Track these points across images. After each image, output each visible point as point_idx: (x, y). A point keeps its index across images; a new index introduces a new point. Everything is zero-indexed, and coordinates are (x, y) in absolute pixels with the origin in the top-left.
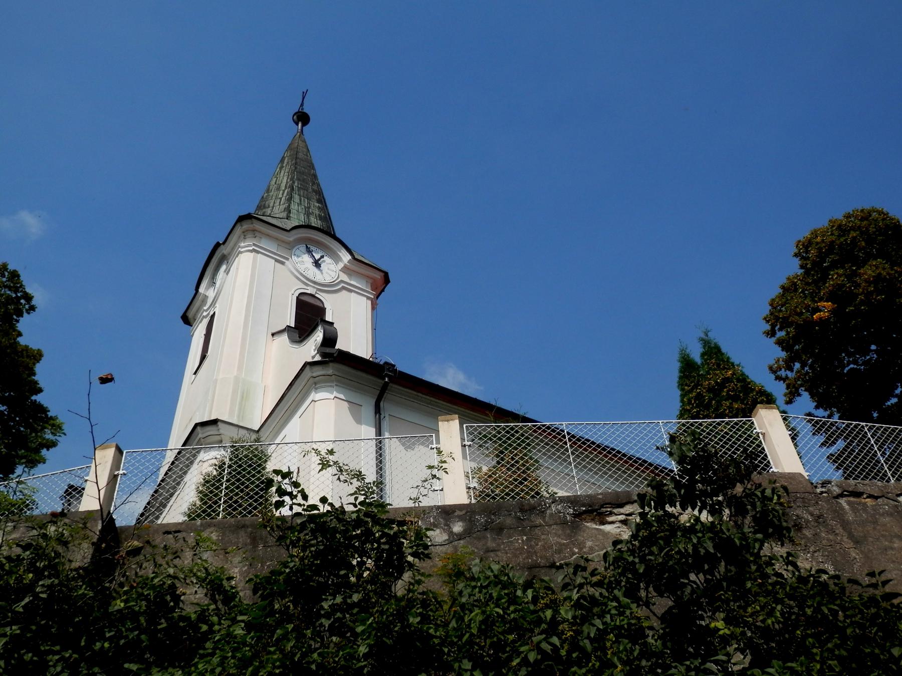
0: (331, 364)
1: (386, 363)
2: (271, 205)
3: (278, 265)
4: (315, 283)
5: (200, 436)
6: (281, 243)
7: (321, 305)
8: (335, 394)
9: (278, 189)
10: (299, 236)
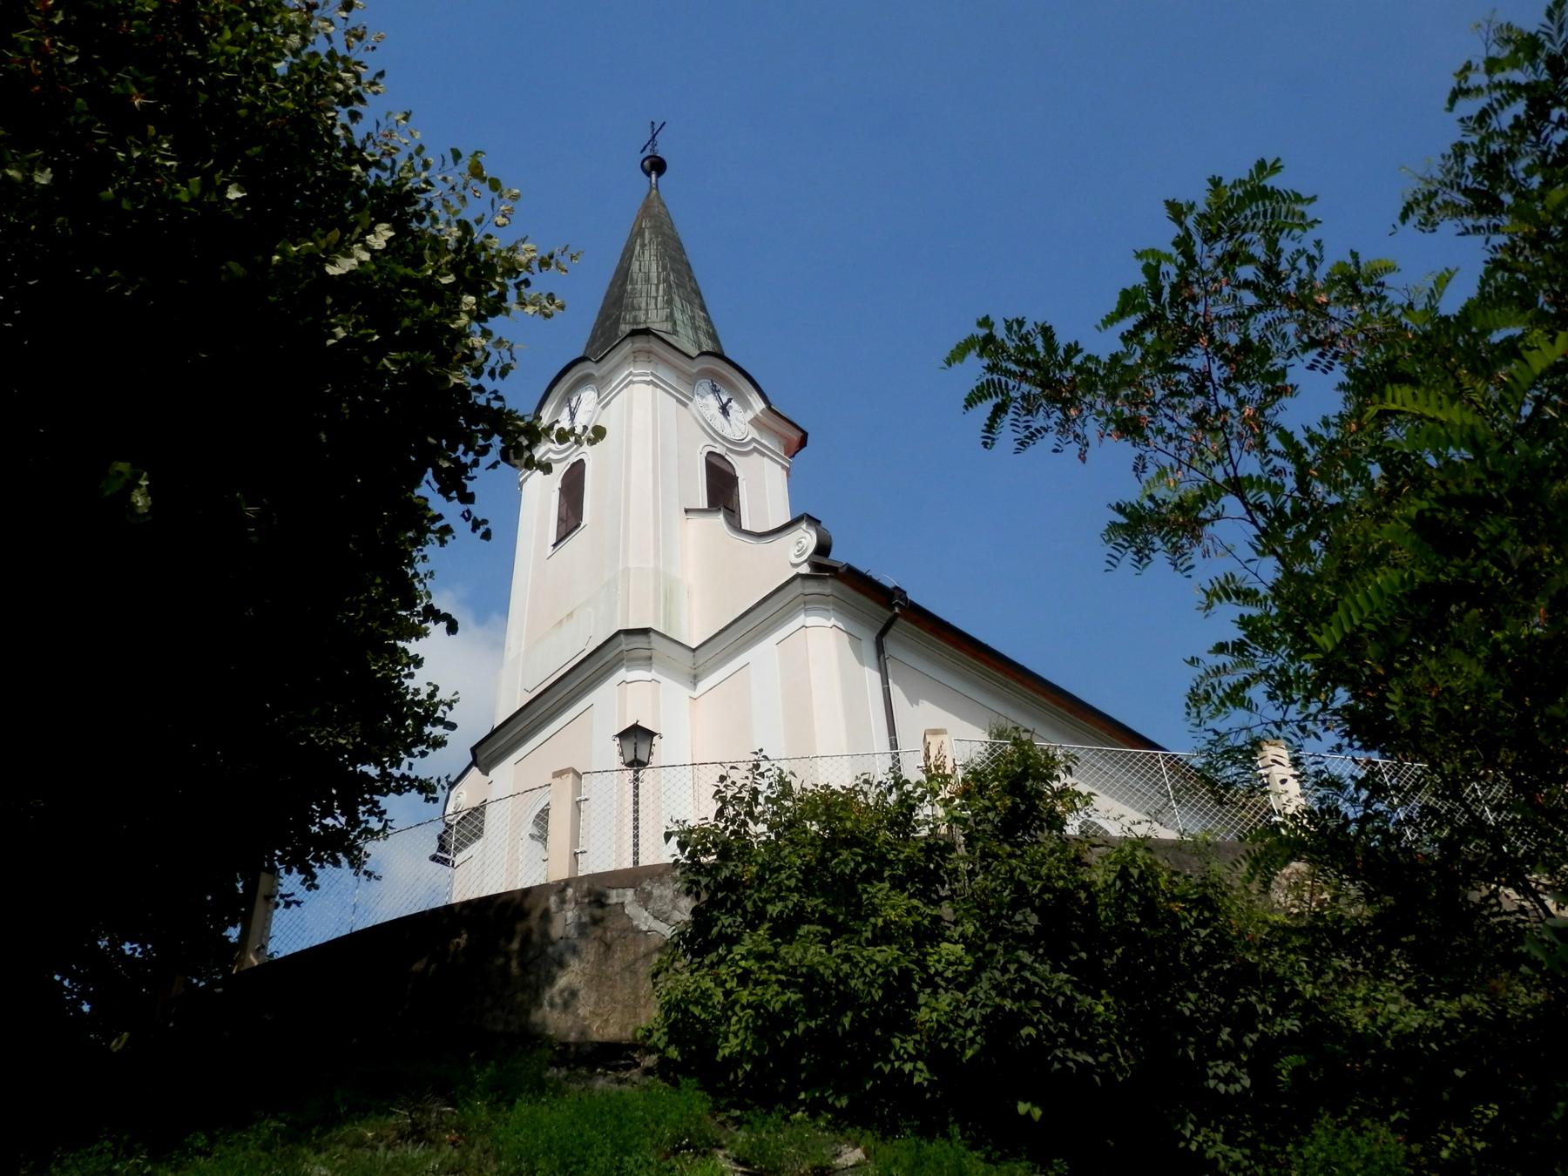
0: (830, 581)
2: (643, 305)
4: (724, 438)
8: (833, 621)
9: (648, 280)
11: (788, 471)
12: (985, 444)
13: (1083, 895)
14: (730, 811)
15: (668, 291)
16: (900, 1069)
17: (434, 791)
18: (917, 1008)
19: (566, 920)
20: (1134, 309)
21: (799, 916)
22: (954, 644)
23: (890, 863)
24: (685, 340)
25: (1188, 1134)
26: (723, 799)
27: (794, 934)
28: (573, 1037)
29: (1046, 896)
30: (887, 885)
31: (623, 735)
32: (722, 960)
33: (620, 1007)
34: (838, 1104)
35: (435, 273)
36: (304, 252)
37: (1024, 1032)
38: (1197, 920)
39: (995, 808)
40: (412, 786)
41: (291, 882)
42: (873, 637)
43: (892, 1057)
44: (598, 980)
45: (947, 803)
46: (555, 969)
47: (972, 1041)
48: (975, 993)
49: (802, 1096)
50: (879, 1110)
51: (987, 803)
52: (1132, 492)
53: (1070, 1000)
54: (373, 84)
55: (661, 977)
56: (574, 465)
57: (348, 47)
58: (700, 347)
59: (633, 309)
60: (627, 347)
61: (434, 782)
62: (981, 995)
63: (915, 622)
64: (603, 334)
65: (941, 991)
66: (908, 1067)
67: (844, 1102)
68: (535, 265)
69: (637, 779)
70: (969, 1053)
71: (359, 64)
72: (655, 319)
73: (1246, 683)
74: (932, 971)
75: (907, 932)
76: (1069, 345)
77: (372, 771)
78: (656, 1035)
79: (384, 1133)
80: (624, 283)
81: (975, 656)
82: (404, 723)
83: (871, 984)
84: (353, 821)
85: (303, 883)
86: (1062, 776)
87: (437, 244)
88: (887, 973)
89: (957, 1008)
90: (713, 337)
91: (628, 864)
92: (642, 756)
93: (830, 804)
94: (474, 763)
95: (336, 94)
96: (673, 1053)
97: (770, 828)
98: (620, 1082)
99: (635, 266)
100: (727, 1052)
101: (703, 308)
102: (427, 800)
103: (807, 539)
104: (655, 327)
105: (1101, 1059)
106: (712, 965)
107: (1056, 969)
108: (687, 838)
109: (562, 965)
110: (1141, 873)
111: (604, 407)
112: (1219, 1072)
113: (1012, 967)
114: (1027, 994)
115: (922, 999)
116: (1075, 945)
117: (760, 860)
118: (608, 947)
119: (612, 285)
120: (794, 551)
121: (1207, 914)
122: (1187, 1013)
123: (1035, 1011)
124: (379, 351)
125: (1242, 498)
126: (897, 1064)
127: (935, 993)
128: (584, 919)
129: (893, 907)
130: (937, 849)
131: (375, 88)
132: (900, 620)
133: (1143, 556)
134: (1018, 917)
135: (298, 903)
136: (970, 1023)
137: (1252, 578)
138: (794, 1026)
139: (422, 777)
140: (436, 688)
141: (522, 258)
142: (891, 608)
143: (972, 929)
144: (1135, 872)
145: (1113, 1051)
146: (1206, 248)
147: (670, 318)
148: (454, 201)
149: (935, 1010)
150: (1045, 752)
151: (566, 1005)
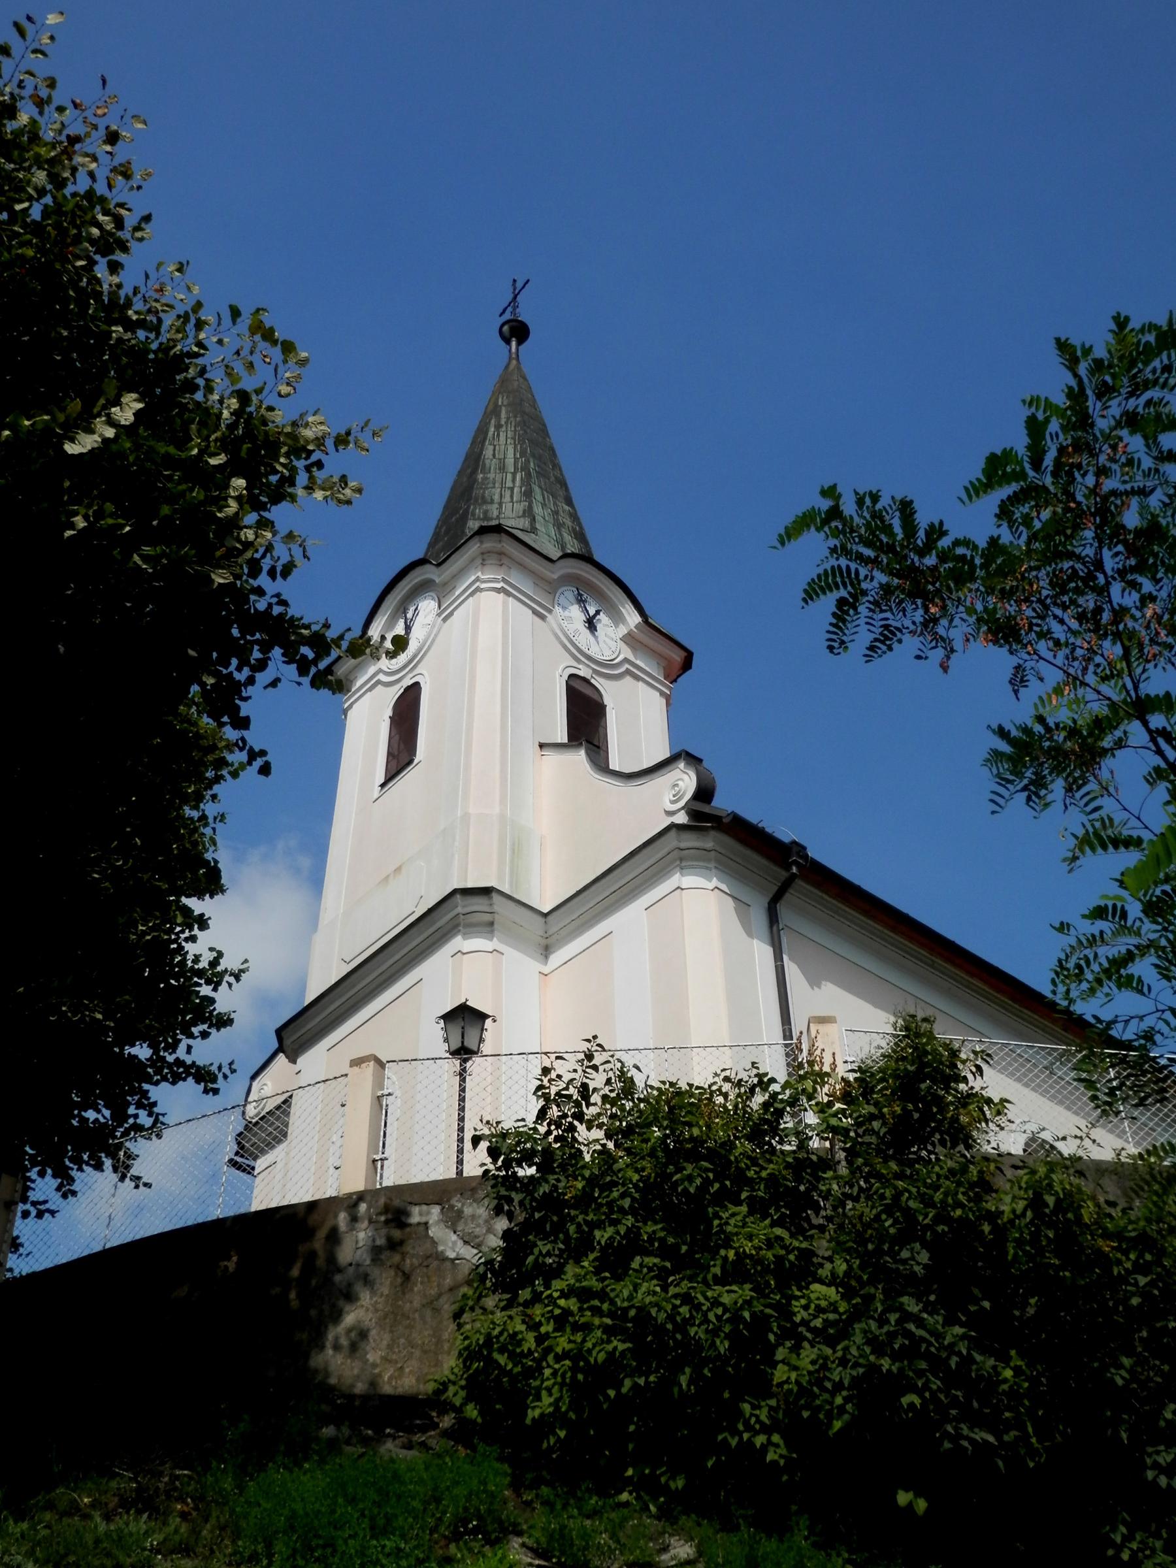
0: (713, 833)
1: (794, 842)
3: (537, 619)
4: (589, 658)
6: (539, 580)
7: (598, 699)
8: (715, 882)
9: (502, 468)
10: (570, 571)
11: (668, 699)
12: (831, 648)
13: (986, 1228)
14: (554, 1112)
15: (527, 481)
16: (750, 1442)
17: (214, 1079)
18: (774, 1365)
19: (357, 1242)
20: (1007, 479)
21: (633, 1245)
22: (865, 913)
23: (750, 1182)
24: (545, 539)
25: (1118, 1539)
26: (546, 1097)
27: (627, 1268)
28: (360, 1388)
29: (940, 1228)
30: (744, 1209)
31: (448, 1017)
32: (536, 1298)
33: (417, 1353)
34: (672, 1485)
35: (202, 452)
36: (39, 427)
37: (905, 1400)
38: (1135, 1263)
39: (882, 1116)
40: (189, 1074)
41: (44, 1187)
42: (764, 901)
43: (741, 1427)
44: (393, 1317)
45: (822, 1109)
46: (341, 1303)
47: (842, 1410)
48: (846, 1349)
49: (630, 1472)
50: (721, 1494)
51: (872, 1109)
52: (1018, 713)
53: (967, 1361)
54: (137, 228)
55: (466, 1317)
56: (408, 689)
57: (110, 187)
58: (563, 548)
59: (485, 502)
60: (474, 548)
61: (214, 1068)
62: (854, 1351)
63: (818, 885)
64: (447, 532)
65: (806, 1344)
66: (760, 1440)
67: (680, 1483)
68: (329, 443)
69: (464, 1070)
70: (837, 1425)
71: (122, 205)
72: (511, 515)
73: (1129, 957)
74: (798, 1319)
75: (766, 1270)
76: (932, 526)
77: (142, 1052)
78: (452, 1389)
79: (104, 1499)
80: (474, 472)
81: (893, 929)
82: (177, 1001)
83: (715, 1333)
84: (120, 1115)
85: (58, 1189)
86: (970, 1077)
87: (208, 418)
88: (736, 1319)
89: (824, 1367)
90: (581, 536)
91: (452, 1174)
92: (471, 1043)
93: (677, 1104)
94: (280, 1049)
95: (92, 241)
96: (472, 1412)
97: (608, 1136)
98: (409, 1446)
99: (488, 452)
100: (537, 1413)
101: (569, 501)
102: (206, 1091)
103: (685, 780)
104: (508, 523)
105: (1006, 1438)
106: (527, 1304)
107: (950, 1321)
108: (503, 1146)
109: (350, 1297)
110: (1058, 1201)
111: (445, 620)
112: (1160, 1460)
113: (893, 1317)
114: (912, 1350)
115: (781, 1353)
116: (976, 1291)
117: (587, 1173)
118: (407, 1277)
119: (460, 473)
120: (668, 796)
121: (1148, 1257)
122: (1120, 1382)
123: (920, 1373)
124: (131, 544)
125: (1145, 724)
126: (746, 1436)
127: (796, 1349)
128: (379, 1242)
129: (750, 1237)
130: (809, 1166)
131: (138, 234)
132: (799, 882)
133: (1035, 790)
134: (905, 1254)
135: (53, 1213)
136: (838, 1387)
137: (1134, 822)
138: (618, 1385)
139: (200, 1063)
140: (220, 955)
141: (308, 433)
142: (787, 868)
143: (844, 1267)
144: (1050, 1200)
145: (1023, 1429)
146: (1099, 405)
147: (529, 513)
148: (238, 367)
149: (796, 1368)
150: (947, 1046)
151: (354, 1347)
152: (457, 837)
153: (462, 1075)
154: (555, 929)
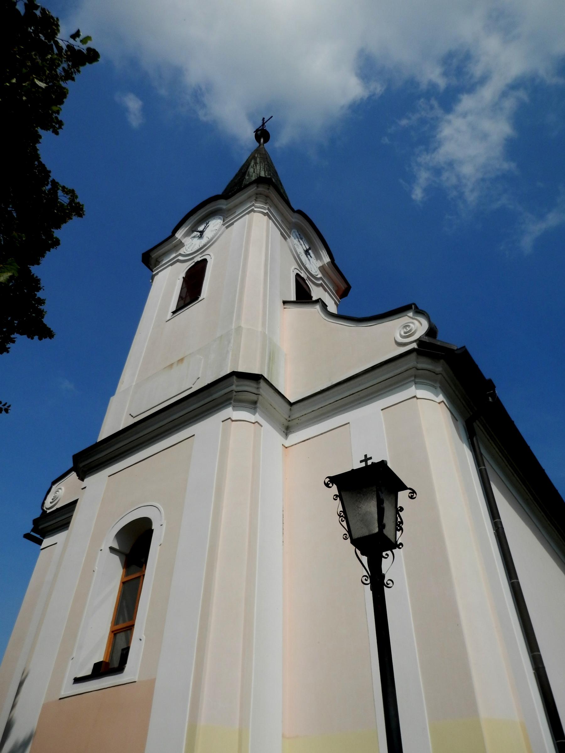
4: (306, 269)
5: (234, 387)
6: (285, 219)
56: (198, 263)
60: (253, 190)
111: (227, 227)
152: (232, 341)
153: (377, 582)
154: (297, 415)
